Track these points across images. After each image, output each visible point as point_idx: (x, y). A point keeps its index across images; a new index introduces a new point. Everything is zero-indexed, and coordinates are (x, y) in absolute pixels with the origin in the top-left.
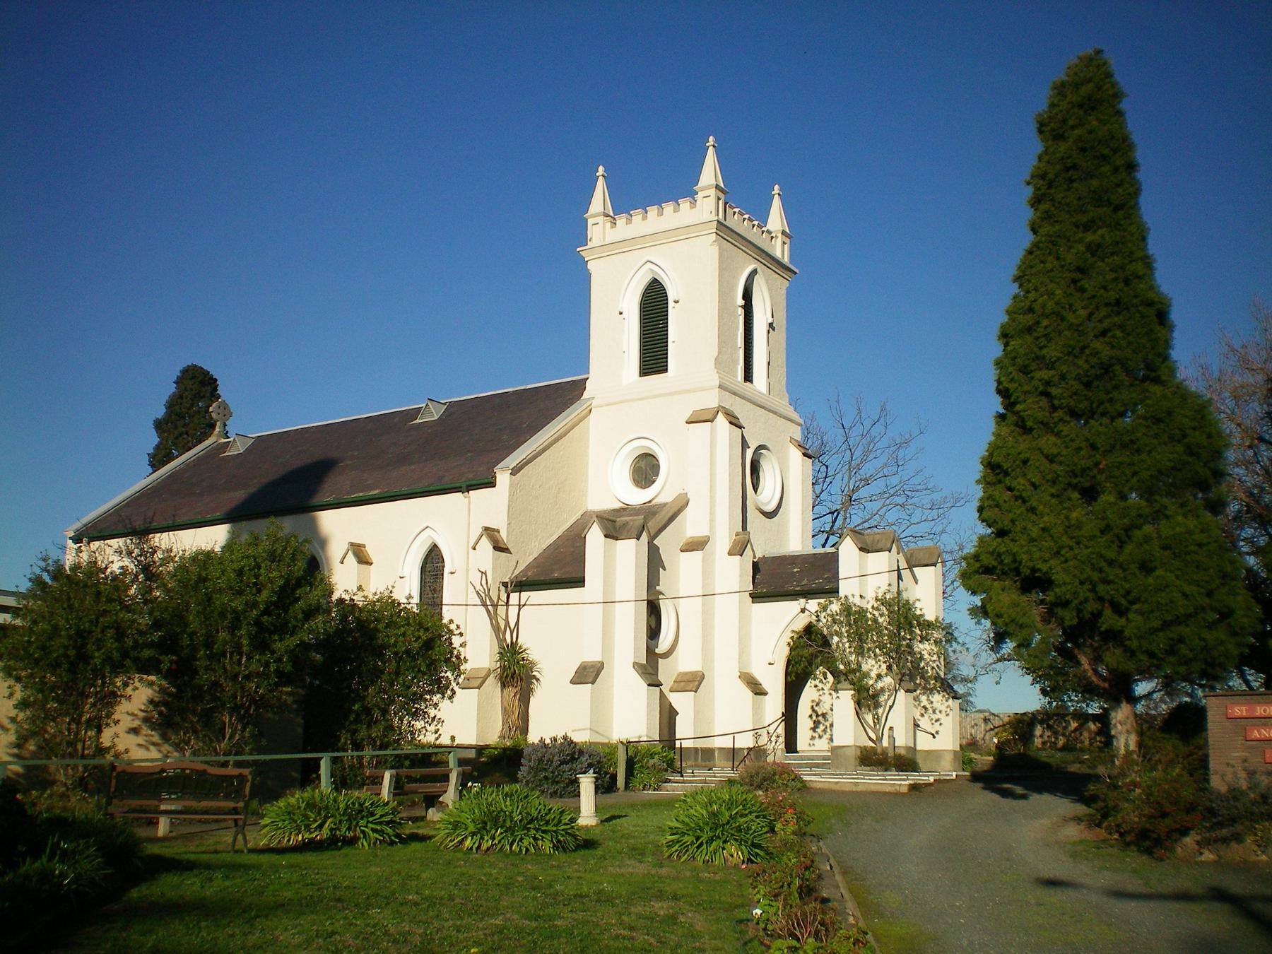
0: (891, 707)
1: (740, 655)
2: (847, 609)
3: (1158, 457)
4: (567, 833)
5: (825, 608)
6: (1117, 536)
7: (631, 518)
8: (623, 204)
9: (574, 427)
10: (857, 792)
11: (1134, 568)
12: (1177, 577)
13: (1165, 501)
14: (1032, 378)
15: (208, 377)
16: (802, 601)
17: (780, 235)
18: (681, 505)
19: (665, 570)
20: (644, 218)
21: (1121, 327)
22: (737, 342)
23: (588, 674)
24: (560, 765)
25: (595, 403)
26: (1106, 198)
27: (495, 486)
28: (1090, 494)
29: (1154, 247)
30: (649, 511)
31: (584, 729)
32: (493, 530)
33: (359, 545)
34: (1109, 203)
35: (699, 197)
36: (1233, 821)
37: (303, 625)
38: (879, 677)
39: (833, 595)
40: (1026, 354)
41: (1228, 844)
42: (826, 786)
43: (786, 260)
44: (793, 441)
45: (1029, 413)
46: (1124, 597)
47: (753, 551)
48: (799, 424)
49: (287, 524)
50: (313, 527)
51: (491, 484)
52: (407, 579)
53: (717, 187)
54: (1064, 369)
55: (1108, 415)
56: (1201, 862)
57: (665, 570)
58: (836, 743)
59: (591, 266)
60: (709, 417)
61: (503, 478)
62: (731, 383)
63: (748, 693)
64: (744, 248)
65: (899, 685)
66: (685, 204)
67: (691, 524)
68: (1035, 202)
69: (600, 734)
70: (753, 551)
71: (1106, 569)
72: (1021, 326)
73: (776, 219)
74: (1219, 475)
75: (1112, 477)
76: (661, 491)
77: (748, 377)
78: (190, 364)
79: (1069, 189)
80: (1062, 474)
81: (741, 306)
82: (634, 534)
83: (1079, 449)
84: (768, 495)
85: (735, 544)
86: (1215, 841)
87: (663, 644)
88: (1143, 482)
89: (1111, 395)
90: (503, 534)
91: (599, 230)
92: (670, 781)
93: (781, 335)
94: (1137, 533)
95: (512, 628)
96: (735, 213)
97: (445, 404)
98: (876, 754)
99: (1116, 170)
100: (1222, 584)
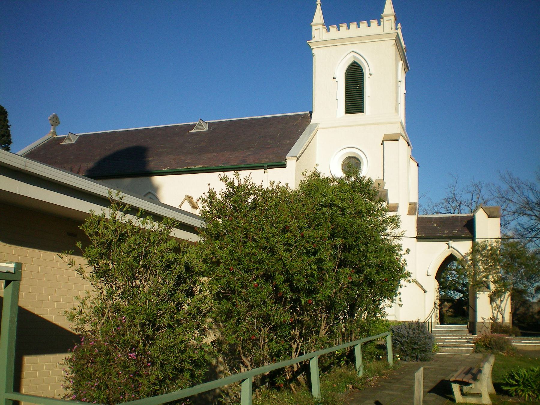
8: (328, 23)
9: (311, 141)
27: (286, 167)
97: (77, 136)
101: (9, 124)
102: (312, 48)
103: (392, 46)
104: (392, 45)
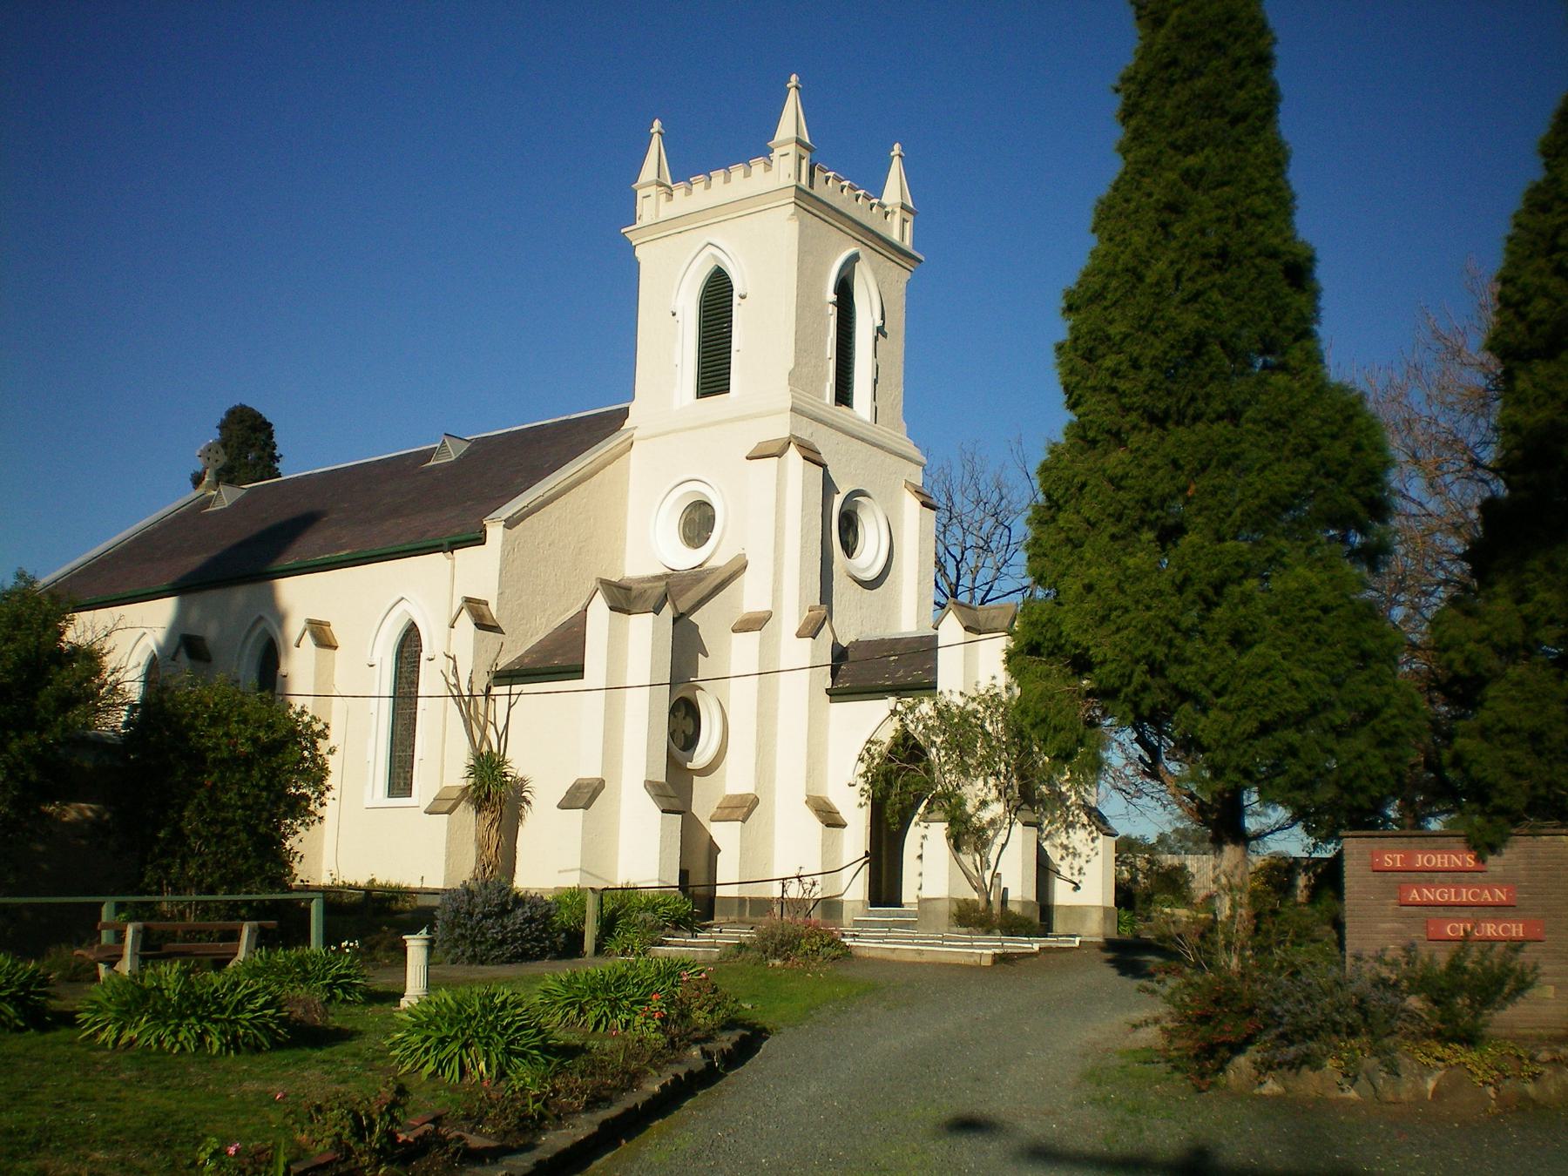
0: (1004, 846)
1: (808, 772)
2: (942, 713)
3: (1272, 478)
4: (252, 1024)
5: (911, 709)
6: (1200, 594)
7: (650, 584)
9: (604, 467)
10: (920, 963)
11: (1222, 641)
12: (1284, 657)
13: (1284, 544)
14: (1099, 368)
15: (259, 421)
16: (892, 700)
17: (898, 210)
18: (738, 569)
19: (707, 656)
20: (708, 187)
21: (1226, 290)
22: (826, 353)
23: (583, 796)
24: (481, 920)
25: (637, 434)
26: (1218, 105)
27: (484, 544)
28: (1169, 535)
29: (1297, 176)
30: (697, 575)
31: (572, 870)
32: (479, 602)
33: (320, 623)
34: (1223, 112)
35: (775, 156)
36: (1312, 1033)
37: (56, 720)
38: (984, 804)
39: (929, 692)
40: (1090, 332)
41: (1298, 1070)
42: (878, 954)
43: (907, 244)
44: (909, 487)
45: (1090, 417)
46: (1207, 684)
47: (833, 631)
48: (919, 464)
49: (240, 596)
50: (271, 601)
51: (480, 540)
52: (377, 668)
53: (799, 142)
54: (1136, 350)
55: (1204, 419)
56: (1262, 1096)
57: (707, 656)
58: (925, 894)
59: (640, 253)
60: (774, 451)
61: (495, 532)
62: (812, 405)
63: (817, 825)
64: (839, 225)
65: (1015, 815)
66: (758, 166)
67: (750, 595)
68: (1125, 117)
69: (598, 877)
70: (833, 631)
71: (1179, 641)
72: (1089, 294)
73: (895, 189)
74: (1379, 509)
75: (1207, 508)
76: (716, 552)
77: (844, 395)
78: (237, 404)
79: (1166, 96)
80: (1130, 504)
81: (833, 303)
82: (651, 604)
83: (1154, 468)
84: (869, 557)
85: (806, 623)
86: (1280, 1065)
87: (703, 753)
88: (1249, 515)
89: (1208, 389)
90: (493, 607)
91: (651, 205)
92: (667, 944)
93: (895, 345)
94: (1234, 590)
95: (500, 733)
96: (827, 179)
98: (976, 910)
99: (1237, 64)
100: (1358, 667)
101: (277, 453)
102: (634, 244)
103: (789, 219)
104: (788, 216)
